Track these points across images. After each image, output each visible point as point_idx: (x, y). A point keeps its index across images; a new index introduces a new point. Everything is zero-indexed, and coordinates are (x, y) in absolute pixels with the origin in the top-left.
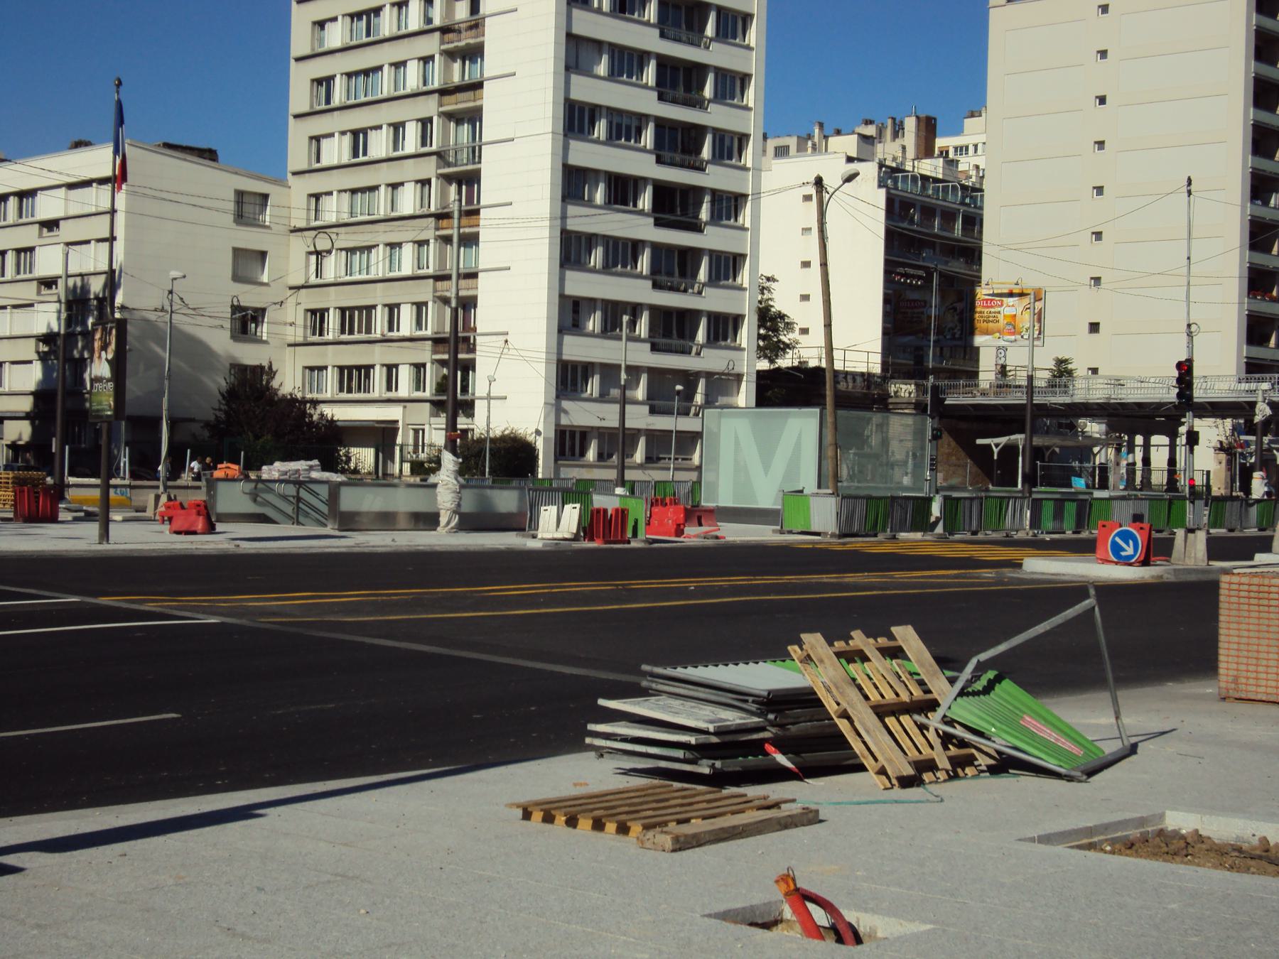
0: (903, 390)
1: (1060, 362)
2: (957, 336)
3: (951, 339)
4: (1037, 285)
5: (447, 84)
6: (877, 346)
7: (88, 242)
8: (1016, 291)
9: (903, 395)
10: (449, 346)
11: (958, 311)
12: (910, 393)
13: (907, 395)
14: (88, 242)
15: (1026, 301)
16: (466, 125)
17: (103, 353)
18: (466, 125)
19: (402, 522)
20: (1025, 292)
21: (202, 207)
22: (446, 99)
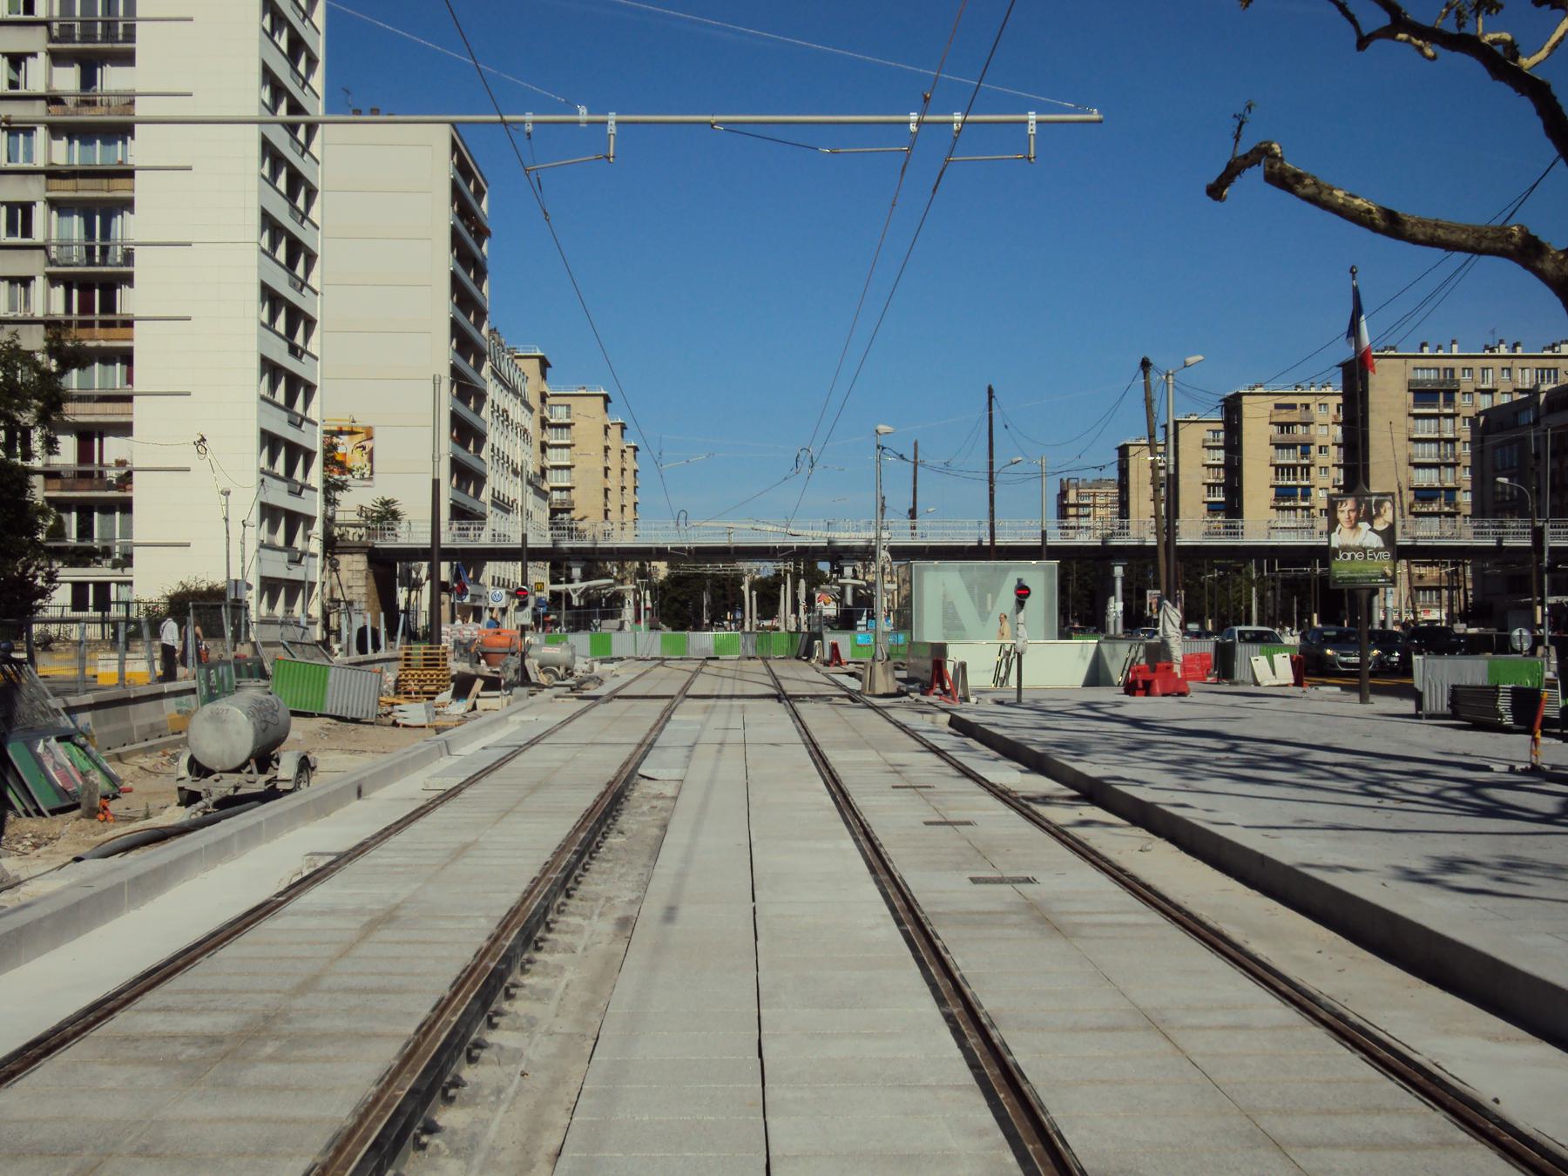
0: (351, 534)
1: (385, 503)
2: (366, 476)
3: (361, 479)
4: (367, 424)
5: (52, 164)
6: (1292, 676)
7: (754, 900)
8: (345, 429)
9: (350, 538)
10: (522, 479)
11: (367, 450)
12: (360, 537)
13: (356, 538)
14: (754, 900)
15: (358, 438)
16: (118, 365)
17: (1272, 614)
18: (118, 365)
19: (118, 325)
20: (355, 430)
21: (228, 532)
22: (56, 183)
